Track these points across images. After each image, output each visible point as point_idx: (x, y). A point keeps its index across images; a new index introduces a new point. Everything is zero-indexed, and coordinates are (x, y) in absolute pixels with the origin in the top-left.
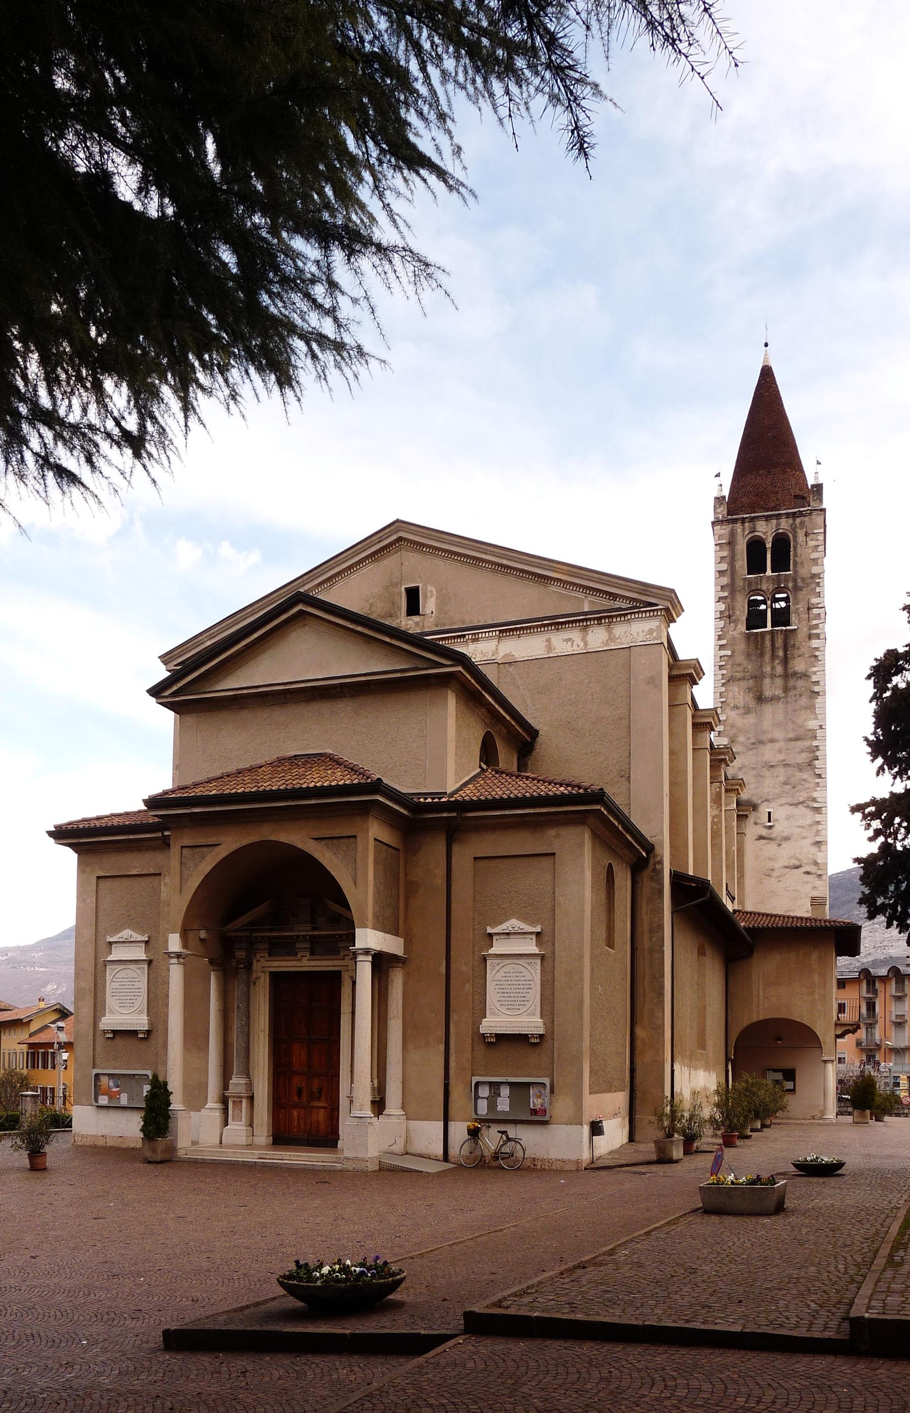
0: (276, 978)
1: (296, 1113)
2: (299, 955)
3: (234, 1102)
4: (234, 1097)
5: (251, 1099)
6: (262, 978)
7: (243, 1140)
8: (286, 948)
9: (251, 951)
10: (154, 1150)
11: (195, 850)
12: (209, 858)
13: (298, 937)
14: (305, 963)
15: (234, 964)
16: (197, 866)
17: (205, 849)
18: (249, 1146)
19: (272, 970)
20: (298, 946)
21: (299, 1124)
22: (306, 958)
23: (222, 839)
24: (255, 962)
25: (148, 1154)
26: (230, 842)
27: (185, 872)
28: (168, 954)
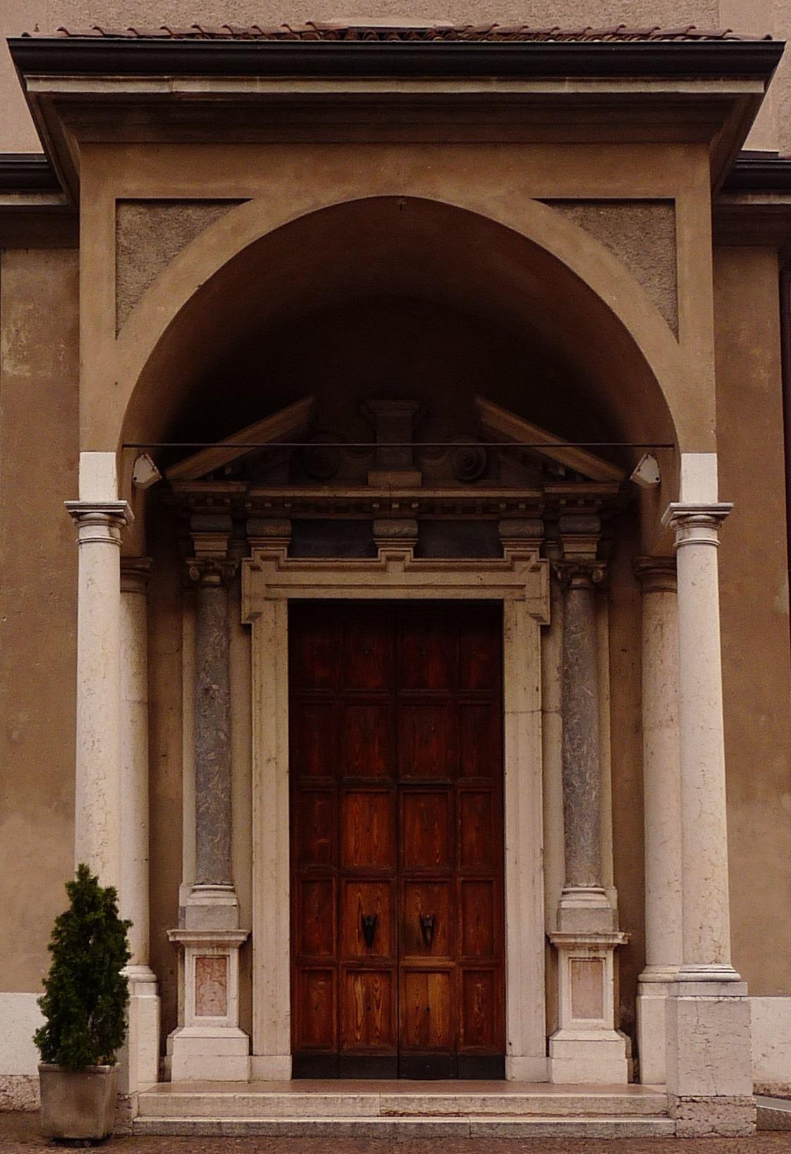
0: (305, 616)
1: (359, 989)
2: (382, 554)
3: (200, 960)
4: (200, 945)
5: (246, 949)
6: (268, 616)
7: (238, 1066)
8: (350, 534)
9: (242, 542)
10: (85, 1105)
11: (163, 213)
12: (210, 237)
13: (385, 503)
14: (397, 578)
15: (194, 572)
16: (167, 262)
17: (193, 213)
18: (251, 1082)
19: (297, 594)
20: (379, 528)
21: (369, 1019)
22: (399, 566)
23: (250, 184)
24: (246, 571)
25: (65, 1118)
26: (278, 196)
27: (133, 277)
28: (79, 515)
